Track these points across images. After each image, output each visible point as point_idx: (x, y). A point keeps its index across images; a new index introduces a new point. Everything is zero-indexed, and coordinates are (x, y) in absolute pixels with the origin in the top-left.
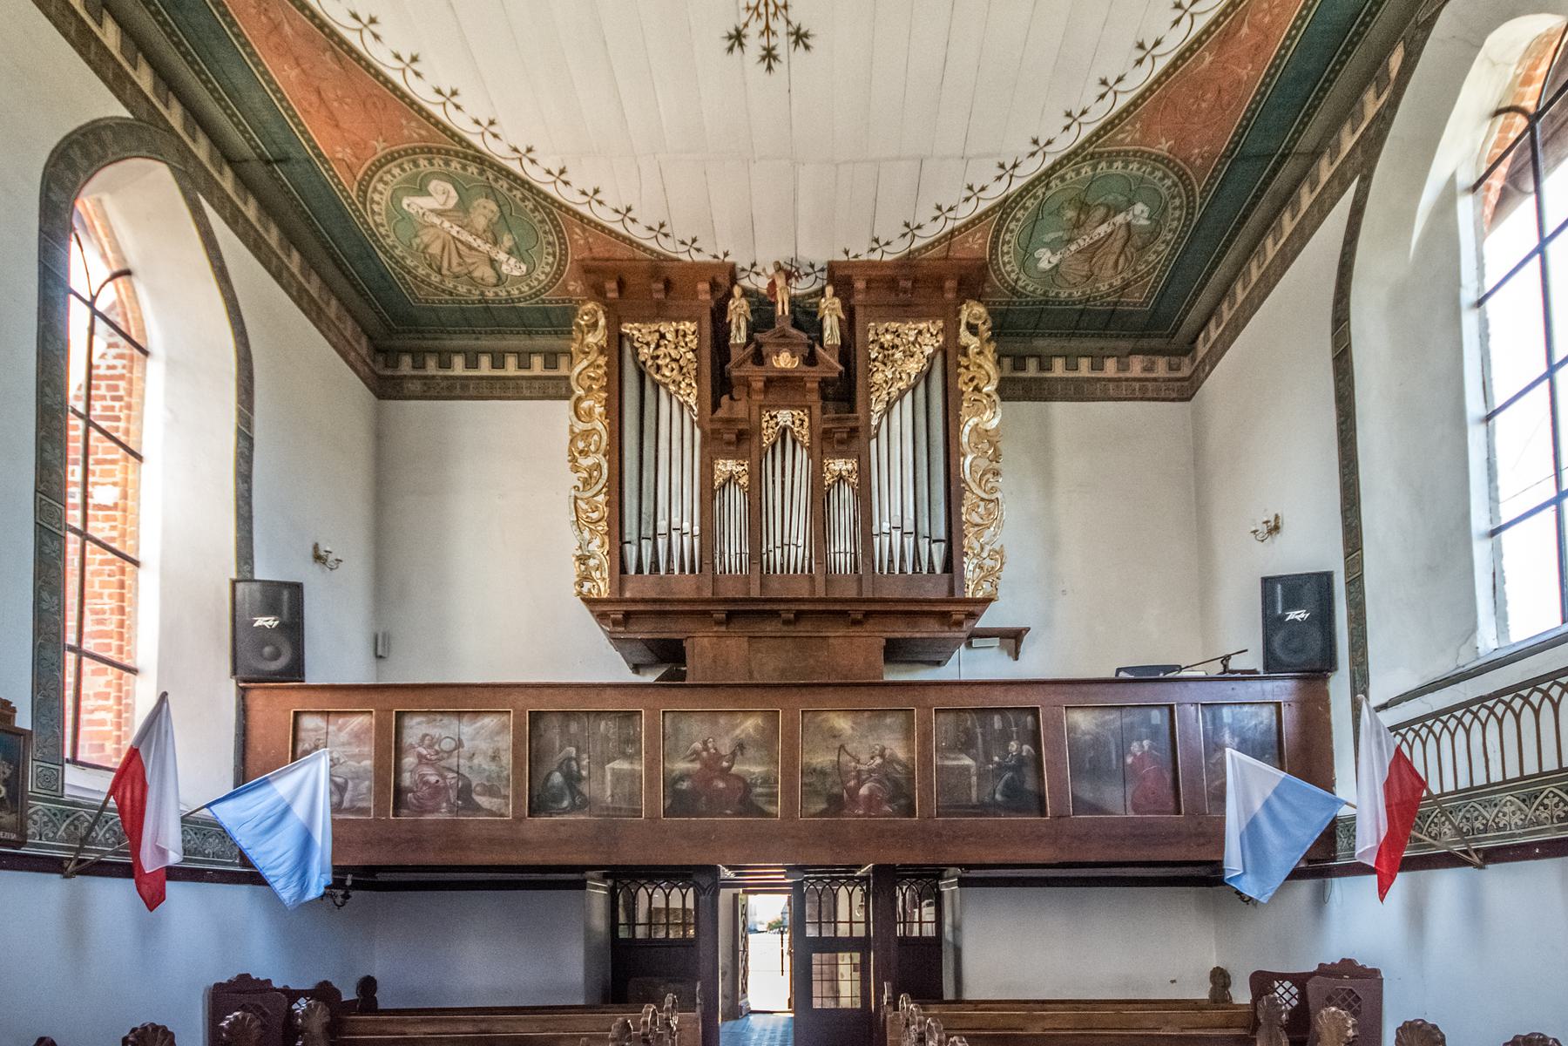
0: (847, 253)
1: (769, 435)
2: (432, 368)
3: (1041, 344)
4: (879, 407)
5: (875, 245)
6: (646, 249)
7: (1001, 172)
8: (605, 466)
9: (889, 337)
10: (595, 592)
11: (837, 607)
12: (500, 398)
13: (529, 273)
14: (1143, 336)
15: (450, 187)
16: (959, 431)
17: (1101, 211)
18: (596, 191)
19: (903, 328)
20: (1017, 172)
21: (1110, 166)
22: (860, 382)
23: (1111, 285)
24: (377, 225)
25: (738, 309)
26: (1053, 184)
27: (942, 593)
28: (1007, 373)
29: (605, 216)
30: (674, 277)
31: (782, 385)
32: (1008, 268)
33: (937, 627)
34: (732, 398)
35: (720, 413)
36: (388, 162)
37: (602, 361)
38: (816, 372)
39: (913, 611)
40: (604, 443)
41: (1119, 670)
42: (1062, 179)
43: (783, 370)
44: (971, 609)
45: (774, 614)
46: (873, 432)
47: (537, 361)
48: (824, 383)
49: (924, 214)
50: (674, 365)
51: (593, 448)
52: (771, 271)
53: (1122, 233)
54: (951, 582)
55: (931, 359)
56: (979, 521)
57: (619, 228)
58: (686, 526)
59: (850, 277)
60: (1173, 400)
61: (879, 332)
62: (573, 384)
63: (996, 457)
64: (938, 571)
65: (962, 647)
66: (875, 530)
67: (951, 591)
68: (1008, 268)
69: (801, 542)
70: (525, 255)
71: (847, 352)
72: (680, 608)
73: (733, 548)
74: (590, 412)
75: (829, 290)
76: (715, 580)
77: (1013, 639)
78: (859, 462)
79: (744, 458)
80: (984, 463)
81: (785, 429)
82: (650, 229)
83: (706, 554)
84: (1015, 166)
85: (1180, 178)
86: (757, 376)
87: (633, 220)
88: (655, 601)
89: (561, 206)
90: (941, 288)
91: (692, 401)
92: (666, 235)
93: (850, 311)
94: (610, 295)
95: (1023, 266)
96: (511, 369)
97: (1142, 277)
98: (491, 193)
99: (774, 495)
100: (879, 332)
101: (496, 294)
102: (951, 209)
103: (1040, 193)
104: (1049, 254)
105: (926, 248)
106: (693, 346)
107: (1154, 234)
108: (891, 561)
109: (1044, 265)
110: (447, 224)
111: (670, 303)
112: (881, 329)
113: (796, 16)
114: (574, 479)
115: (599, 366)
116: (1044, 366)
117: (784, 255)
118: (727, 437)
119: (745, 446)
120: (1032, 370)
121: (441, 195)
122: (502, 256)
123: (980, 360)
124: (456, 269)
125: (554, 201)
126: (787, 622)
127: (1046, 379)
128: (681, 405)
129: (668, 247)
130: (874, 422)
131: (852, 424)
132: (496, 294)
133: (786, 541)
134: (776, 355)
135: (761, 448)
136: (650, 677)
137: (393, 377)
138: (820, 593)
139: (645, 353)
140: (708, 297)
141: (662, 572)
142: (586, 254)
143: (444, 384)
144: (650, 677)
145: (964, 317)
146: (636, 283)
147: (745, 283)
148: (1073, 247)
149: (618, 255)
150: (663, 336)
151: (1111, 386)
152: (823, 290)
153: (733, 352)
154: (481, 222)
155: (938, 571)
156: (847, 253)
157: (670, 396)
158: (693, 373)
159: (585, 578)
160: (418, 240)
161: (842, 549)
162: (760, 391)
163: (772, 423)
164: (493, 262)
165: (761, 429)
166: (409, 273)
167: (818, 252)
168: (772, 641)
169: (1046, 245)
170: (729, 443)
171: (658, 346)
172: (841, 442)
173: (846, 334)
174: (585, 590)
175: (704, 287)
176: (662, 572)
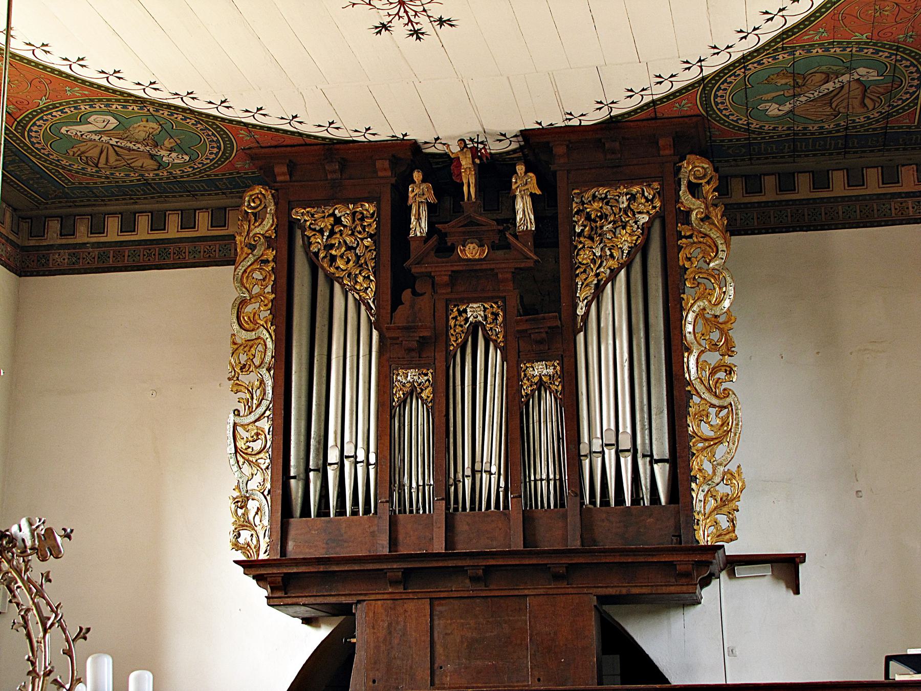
8: (269, 383)
9: (596, 205)
16: (681, 319)
17: (819, 77)
31: (473, 282)
34: (414, 293)
37: (270, 255)
40: (269, 354)
46: (580, 323)
51: (257, 361)
55: (647, 229)
56: (712, 434)
58: (361, 456)
63: (729, 350)
64: (663, 500)
66: (584, 450)
69: (494, 469)
73: (417, 477)
78: (562, 365)
80: (713, 358)
81: (475, 326)
86: (441, 270)
88: (319, 561)
100: (592, 200)
113: (436, 11)
115: (267, 261)
116: (821, 180)
118: (412, 343)
123: (705, 228)
130: (580, 312)
135: (447, 351)
137: (37, 248)
139: (318, 242)
150: (338, 221)
153: (413, 245)
158: (372, 264)
159: (245, 524)
161: (544, 470)
164: (152, 157)
165: (448, 327)
171: (332, 233)
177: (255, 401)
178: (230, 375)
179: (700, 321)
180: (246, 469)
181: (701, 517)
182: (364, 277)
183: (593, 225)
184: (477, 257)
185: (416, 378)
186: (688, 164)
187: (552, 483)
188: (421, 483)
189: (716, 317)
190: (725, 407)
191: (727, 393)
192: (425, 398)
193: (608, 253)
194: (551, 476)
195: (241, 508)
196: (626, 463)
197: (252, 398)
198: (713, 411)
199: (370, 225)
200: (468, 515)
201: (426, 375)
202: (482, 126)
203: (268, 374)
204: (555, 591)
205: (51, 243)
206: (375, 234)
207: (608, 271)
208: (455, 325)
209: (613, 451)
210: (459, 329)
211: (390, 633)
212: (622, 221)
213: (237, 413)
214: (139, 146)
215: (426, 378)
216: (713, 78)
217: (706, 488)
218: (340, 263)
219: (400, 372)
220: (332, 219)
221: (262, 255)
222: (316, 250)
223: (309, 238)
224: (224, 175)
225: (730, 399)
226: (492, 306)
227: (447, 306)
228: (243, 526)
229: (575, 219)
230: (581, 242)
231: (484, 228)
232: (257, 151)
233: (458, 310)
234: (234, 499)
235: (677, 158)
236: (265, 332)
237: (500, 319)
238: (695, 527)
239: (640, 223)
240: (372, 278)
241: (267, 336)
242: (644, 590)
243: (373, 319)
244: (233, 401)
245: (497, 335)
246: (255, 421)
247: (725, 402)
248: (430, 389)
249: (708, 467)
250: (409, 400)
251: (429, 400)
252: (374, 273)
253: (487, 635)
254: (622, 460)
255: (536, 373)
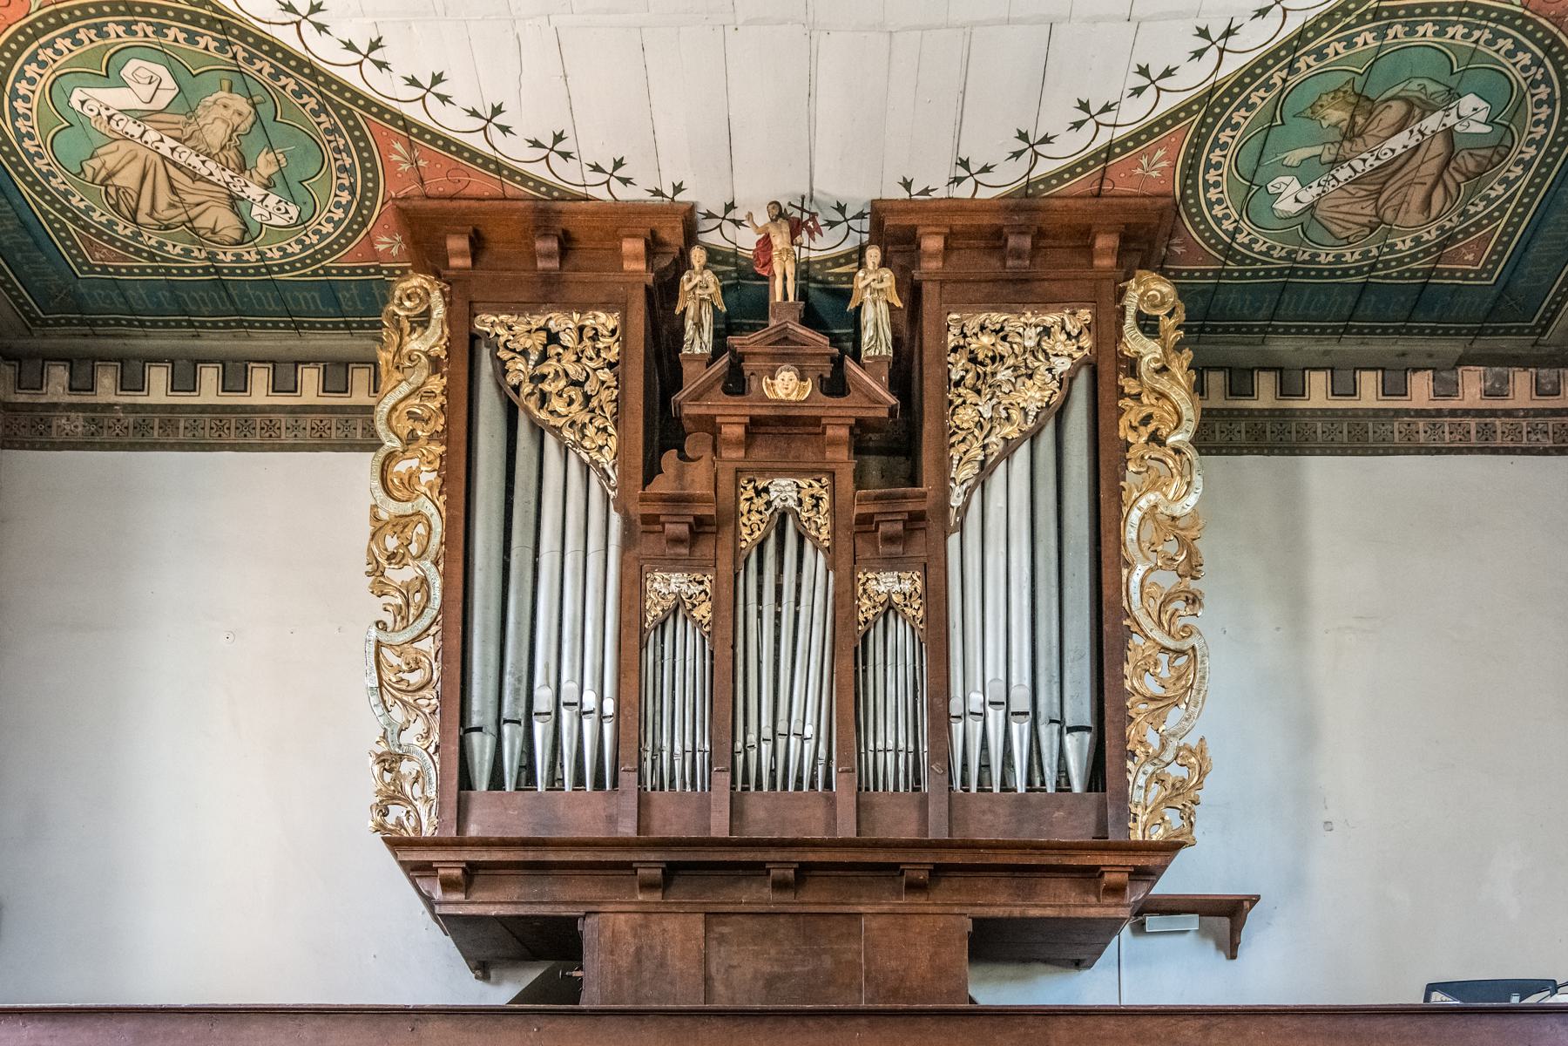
0: (907, 185)
1: (752, 525)
2: (107, 389)
3: (1284, 346)
4: (967, 472)
5: (962, 172)
6: (526, 179)
7: (1202, 43)
8: (437, 583)
9: (986, 340)
10: (410, 824)
11: (881, 857)
12: (234, 447)
13: (301, 222)
14: (1481, 332)
15: (161, 71)
16: (1119, 519)
17: (1397, 110)
18: (437, 79)
19: (1013, 322)
20: (1232, 43)
21: (1412, 32)
22: (929, 427)
23: (1418, 241)
24: (20, 137)
25: (700, 289)
26: (1301, 64)
27: (1085, 835)
28: (1217, 401)
29: (451, 121)
30: (576, 225)
32: (1218, 211)
33: (1073, 897)
34: (683, 457)
35: (663, 485)
36: (50, 28)
37: (437, 384)
38: (848, 408)
39: (1027, 866)
40: (436, 540)
41: (1431, 988)
42: (1320, 54)
43: (780, 404)
44: (1141, 861)
45: (756, 869)
46: (953, 518)
47: (310, 378)
48: (861, 427)
49: (1056, 116)
50: (574, 393)
51: (414, 549)
52: (762, 219)
53: (1438, 146)
54: (1102, 808)
55: (1066, 382)
56: (1160, 692)
57: (477, 142)
58: (590, 700)
59: (914, 228)
60: (1545, 452)
61: (970, 329)
62: (381, 427)
63: (1192, 569)
64: (1077, 787)
65: (1126, 931)
66: (956, 707)
67: (1102, 826)
68: (1218, 211)
69: (809, 731)
70: (295, 187)
71: (904, 373)
72: (571, 856)
73: (680, 737)
74: (410, 480)
75: (873, 255)
76: (643, 803)
77: (1226, 917)
79: (703, 569)
82: (536, 144)
83: (629, 752)
84: (1229, 33)
85: (1547, 51)
87: (505, 129)
88: (525, 843)
89: (369, 104)
90: (1088, 250)
91: (606, 459)
92: (566, 155)
93: (912, 293)
94: (456, 262)
95: (1245, 208)
96: (259, 393)
97: (1478, 225)
98: (239, 80)
99: (760, 638)
100: (970, 329)
101: (239, 257)
102: (1107, 108)
103: (1277, 80)
104: (1296, 186)
105: (1059, 176)
106: (612, 356)
107: (1499, 149)
108: (985, 766)
109: (1286, 205)
110: (152, 136)
111: (570, 276)
112: (972, 325)
114: (376, 608)
115: (431, 395)
116: (1290, 385)
117: (788, 189)
119: (705, 549)
120: (1265, 396)
121: (144, 84)
122: (254, 192)
123: (1163, 383)
124: (164, 213)
125: (356, 96)
126: (780, 885)
127: (1292, 412)
128: (586, 468)
129: (569, 175)
130: (956, 501)
131: (911, 506)
132: (239, 257)
133: (782, 727)
134: (762, 373)
135: (737, 550)
136: (501, 993)
137: (32, 407)
138: (847, 830)
139: (519, 370)
140: (642, 266)
141: (541, 786)
142: (413, 188)
143: (131, 419)
144: (501, 993)
145: (1132, 302)
146: (504, 239)
147: (714, 239)
148: (1344, 174)
149: (472, 190)
151: (1421, 424)
152: (861, 250)
153: (688, 369)
154: (216, 134)
155: (1077, 787)
156: (907, 185)
157: (565, 451)
158: (609, 408)
159: (393, 796)
160: (96, 163)
161: (891, 737)
162: (737, 444)
163: (759, 503)
164: (234, 201)
165: (737, 514)
166: (75, 219)
167: (851, 179)
168: (749, 923)
169: (1290, 170)
170: (676, 541)
171: (544, 357)
172: (890, 539)
173: (906, 334)
174: (390, 820)
175: (633, 245)
176: (541, 786)
177: (412, 610)
178: (369, 568)
179: (1150, 525)
180: (398, 714)
181: (1139, 811)
182: (598, 429)
183: (980, 369)
184: (793, 397)
185: (684, 587)
186: (1139, 284)
187: (902, 756)
188: (689, 746)
189: (1174, 518)
190: (1183, 653)
191: (1188, 631)
192: (699, 617)
193: (1004, 414)
194: (902, 745)
195: (390, 771)
196: (1020, 730)
197: (408, 605)
198: (1164, 658)
199: (609, 348)
200: (764, 796)
201: (701, 583)
202: (812, 189)
203: (434, 569)
204: (907, 909)
205: (55, 400)
206: (617, 363)
207: (1002, 443)
208: (749, 511)
209: (1001, 713)
210: (755, 517)
211: (639, 962)
212: (1027, 367)
213: (381, 625)
214: (211, 165)
215: (701, 588)
216: (1228, 92)
217: (1150, 769)
218: (558, 404)
219: (658, 575)
220: (544, 334)
221: (424, 384)
222: (516, 382)
223: (504, 363)
224: (353, 271)
225: (1193, 641)
226: (810, 486)
227: (737, 480)
228: (393, 798)
229: (950, 359)
230: (959, 396)
231: (808, 350)
232: (417, 203)
233: (755, 488)
234: (378, 756)
235: (1121, 274)
236: (428, 503)
237: (825, 505)
238: (1131, 824)
239: (1057, 371)
240: (610, 430)
241: (431, 509)
242: (1049, 912)
243: (612, 494)
244: (376, 608)
245: (818, 529)
246: (413, 641)
247: (1186, 645)
248: (708, 604)
249: (1153, 740)
250: (670, 621)
251: (705, 621)
252: (616, 423)
253: (797, 969)
254: (1015, 727)
255: (882, 588)
